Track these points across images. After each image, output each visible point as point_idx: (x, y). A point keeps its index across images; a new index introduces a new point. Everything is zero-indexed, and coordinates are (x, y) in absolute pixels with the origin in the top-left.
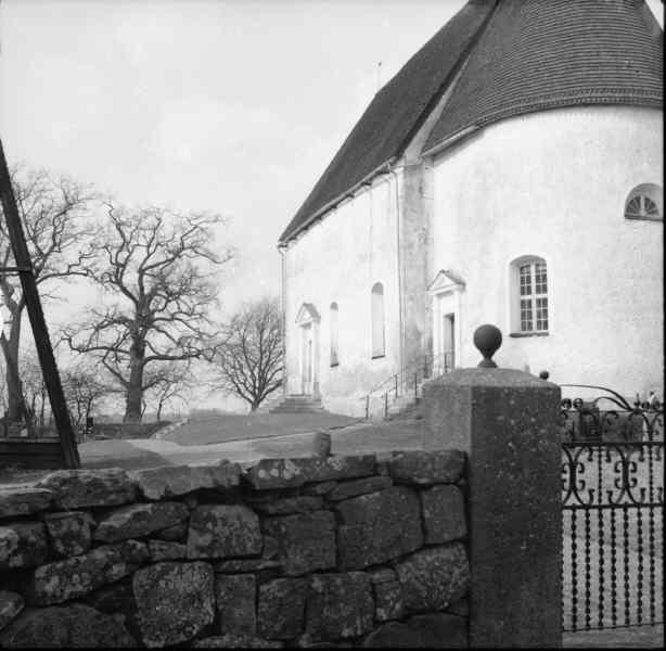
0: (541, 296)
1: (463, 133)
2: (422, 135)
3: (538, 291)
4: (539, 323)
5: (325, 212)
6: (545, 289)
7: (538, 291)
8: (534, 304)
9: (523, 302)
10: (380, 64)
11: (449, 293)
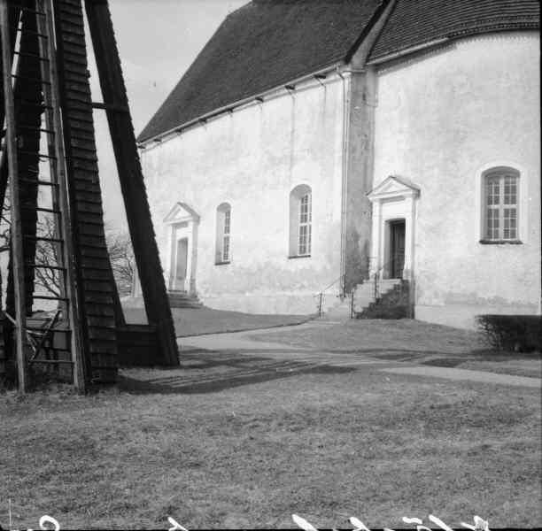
1: (425, 45)
2: (366, 45)
3: (506, 202)
4: (506, 232)
5: (209, 117)
6: (514, 201)
7: (506, 202)
8: (502, 200)
11: (401, 198)
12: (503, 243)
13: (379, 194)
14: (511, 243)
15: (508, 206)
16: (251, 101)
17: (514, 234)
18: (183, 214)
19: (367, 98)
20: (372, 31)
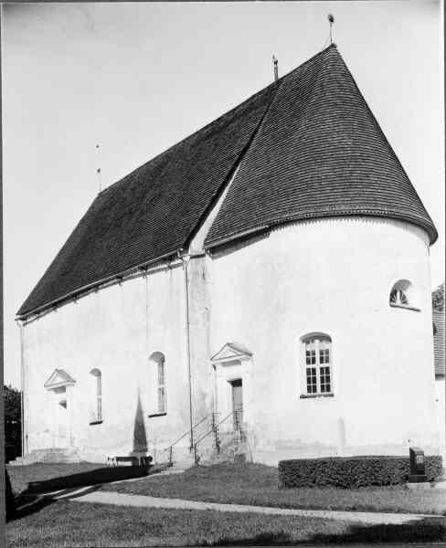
0: (311, 366)
3: (314, 370)
4: (323, 387)
6: (308, 371)
8: (318, 372)
9: (327, 361)
10: (99, 171)
12: (320, 396)
13: (220, 359)
14: (326, 396)
15: (322, 365)
16: (113, 279)
17: (328, 389)
18: (59, 380)
19: (207, 277)
20: (209, 218)
